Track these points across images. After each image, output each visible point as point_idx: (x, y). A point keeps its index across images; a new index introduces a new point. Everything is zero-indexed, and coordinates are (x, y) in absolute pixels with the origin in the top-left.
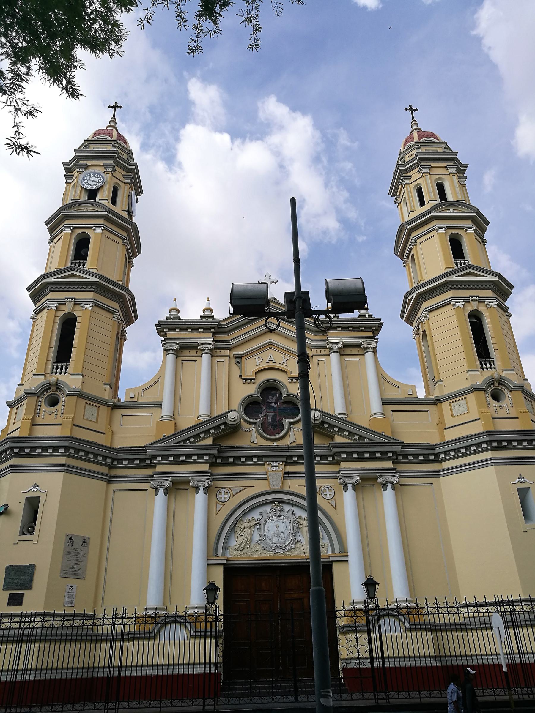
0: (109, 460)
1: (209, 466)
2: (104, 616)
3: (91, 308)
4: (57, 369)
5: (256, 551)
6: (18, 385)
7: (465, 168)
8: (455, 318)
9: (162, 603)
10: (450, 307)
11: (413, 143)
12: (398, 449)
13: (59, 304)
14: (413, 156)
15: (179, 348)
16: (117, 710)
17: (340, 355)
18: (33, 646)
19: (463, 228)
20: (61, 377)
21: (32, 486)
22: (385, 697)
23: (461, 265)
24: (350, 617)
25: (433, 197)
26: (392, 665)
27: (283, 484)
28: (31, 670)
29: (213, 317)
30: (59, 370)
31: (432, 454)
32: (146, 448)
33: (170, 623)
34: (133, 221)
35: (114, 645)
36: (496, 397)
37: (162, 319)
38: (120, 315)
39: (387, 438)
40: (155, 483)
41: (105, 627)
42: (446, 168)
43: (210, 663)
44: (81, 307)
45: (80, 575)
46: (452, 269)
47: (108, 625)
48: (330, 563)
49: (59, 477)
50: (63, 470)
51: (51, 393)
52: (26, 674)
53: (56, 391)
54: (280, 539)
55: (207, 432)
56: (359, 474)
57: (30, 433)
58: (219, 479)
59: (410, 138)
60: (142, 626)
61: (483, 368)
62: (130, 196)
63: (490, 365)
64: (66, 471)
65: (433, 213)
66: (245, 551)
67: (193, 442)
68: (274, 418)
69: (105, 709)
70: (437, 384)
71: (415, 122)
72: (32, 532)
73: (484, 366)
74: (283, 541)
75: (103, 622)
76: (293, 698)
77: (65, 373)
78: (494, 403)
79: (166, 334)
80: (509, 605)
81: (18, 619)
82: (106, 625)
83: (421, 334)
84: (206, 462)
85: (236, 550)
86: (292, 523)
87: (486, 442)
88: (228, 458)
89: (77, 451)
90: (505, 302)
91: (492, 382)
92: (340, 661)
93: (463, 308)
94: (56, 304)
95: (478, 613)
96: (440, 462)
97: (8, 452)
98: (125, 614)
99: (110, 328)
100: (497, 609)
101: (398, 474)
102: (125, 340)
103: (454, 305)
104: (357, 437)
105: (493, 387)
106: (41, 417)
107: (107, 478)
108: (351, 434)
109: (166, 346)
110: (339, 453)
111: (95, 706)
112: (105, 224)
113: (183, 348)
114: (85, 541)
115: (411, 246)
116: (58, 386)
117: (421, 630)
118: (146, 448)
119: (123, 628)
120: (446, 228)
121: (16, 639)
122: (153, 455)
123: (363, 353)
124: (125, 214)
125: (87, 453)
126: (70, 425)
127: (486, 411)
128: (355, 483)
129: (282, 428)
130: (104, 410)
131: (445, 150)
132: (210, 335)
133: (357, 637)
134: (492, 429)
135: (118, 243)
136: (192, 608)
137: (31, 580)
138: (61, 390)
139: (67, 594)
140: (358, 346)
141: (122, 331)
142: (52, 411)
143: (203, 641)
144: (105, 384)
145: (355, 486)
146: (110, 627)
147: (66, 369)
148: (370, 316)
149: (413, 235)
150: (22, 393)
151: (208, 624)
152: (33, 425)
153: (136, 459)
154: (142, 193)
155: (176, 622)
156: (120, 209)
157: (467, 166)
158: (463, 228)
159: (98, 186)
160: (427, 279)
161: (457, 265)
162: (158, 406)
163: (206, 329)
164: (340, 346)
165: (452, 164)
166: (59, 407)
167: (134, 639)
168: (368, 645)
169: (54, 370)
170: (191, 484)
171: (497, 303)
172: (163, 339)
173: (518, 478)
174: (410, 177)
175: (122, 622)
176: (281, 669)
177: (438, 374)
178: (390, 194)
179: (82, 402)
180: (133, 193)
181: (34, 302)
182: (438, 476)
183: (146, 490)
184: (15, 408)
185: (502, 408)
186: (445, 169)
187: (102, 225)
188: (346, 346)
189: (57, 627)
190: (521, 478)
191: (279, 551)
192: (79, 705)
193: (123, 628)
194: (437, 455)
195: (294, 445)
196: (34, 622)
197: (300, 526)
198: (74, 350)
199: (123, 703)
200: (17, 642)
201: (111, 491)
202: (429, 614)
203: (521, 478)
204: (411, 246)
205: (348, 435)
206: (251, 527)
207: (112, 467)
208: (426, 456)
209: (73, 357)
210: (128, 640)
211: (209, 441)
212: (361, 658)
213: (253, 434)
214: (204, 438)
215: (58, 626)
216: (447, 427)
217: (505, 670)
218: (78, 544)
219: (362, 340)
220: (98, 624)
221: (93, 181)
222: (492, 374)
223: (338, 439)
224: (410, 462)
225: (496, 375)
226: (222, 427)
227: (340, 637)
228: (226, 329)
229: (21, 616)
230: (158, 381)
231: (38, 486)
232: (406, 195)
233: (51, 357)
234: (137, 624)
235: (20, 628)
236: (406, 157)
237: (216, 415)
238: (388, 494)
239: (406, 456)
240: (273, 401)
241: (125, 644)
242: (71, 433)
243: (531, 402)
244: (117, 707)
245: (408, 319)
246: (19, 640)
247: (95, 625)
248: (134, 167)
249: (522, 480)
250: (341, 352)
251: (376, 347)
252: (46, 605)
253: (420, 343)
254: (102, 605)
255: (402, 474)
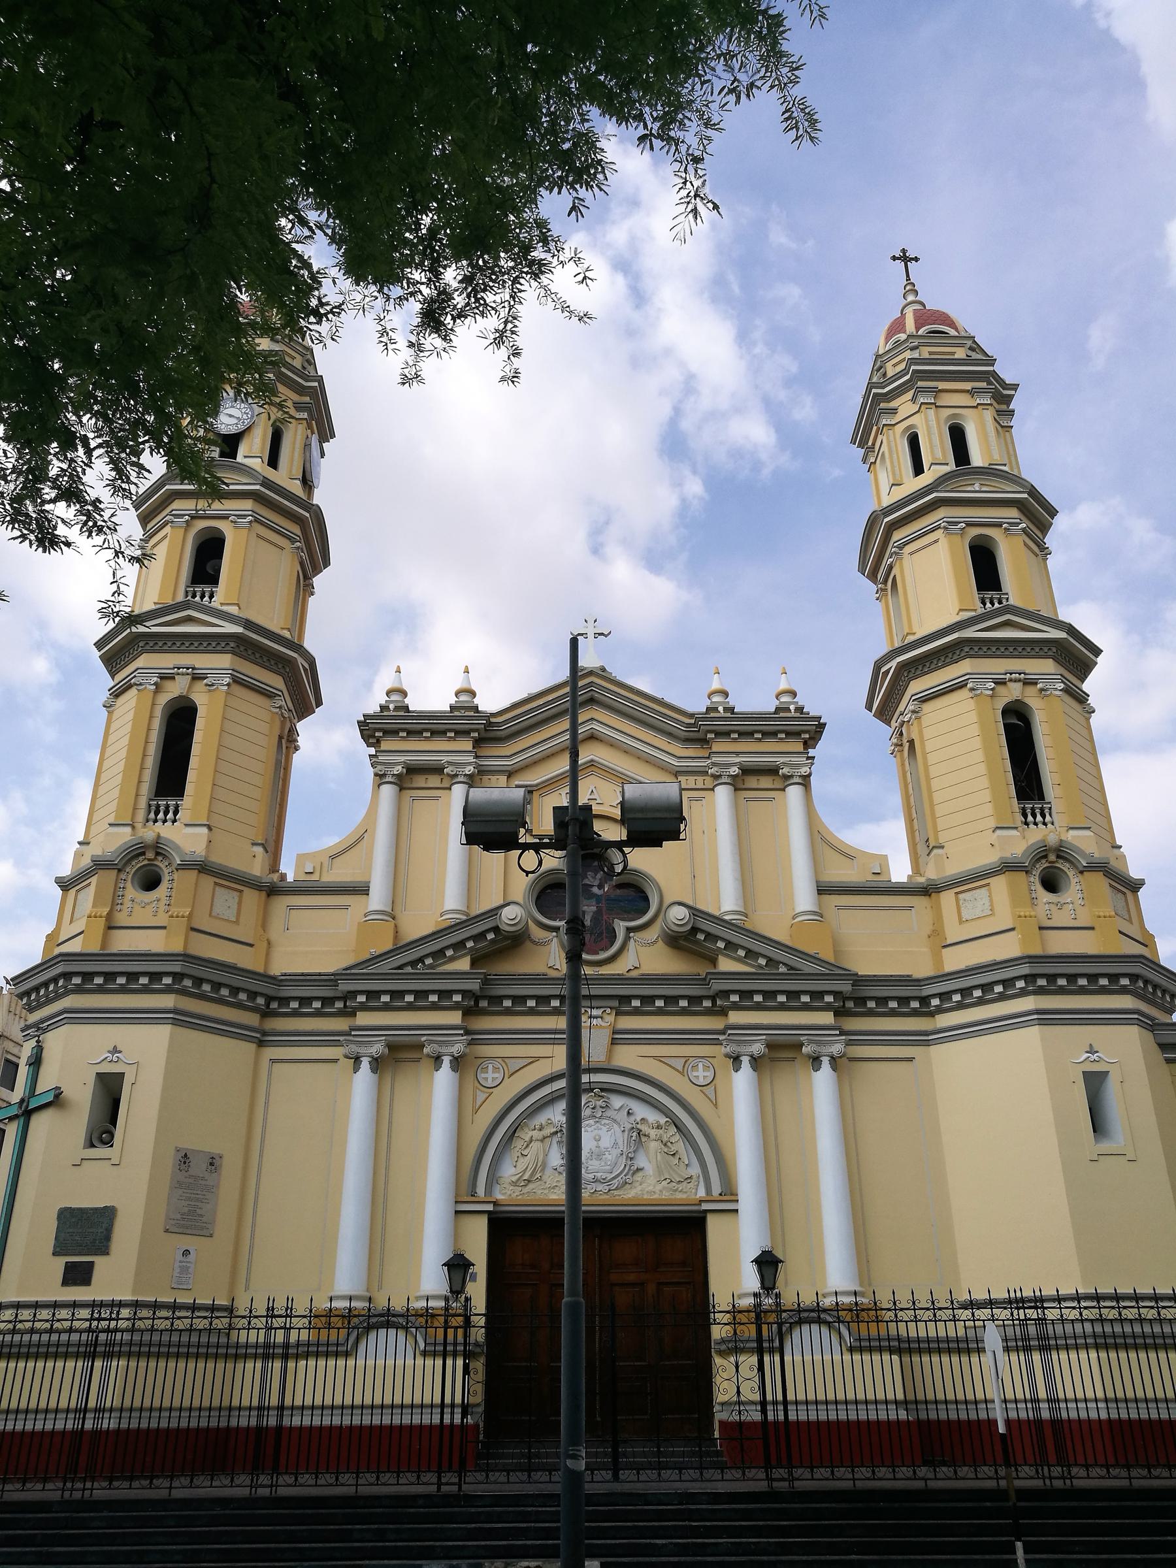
0: (261, 1001)
1: (464, 1015)
2: (251, 1311)
3: (226, 688)
4: (157, 813)
5: (554, 1188)
6: (80, 843)
7: (1013, 392)
8: (973, 717)
9: (365, 1288)
10: (964, 694)
11: (903, 337)
12: (846, 987)
13: (161, 678)
14: (902, 366)
15: (405, 770)
16: (274, 1488)
17: (736, 790)
18: (114, 1363)
19: (999, 525)
20: (165, 831)
21: (109, 1052)
22: (786, 1476)
23: (993, 604)
24: (726, 1324)
25: (939, 456)
26: (803, 1417)
27: (610, 1053)
28: (111, 1410)
29: (476, 709)
30: (161, 815)
31: (915, 998)
32: (337, 977)
33: (377, 1327)
34: (314, 503)
35: (270, 1365)
36: (1051, 884)
37: (371, 712)
38: (285, 701)
39: (823, 965)
40: (354, 1048)
41: (253, 1333)
42: (972, 393)
43: (453, 1406)
44: (207, 685)
45: (202, 1228)
46: (973, 614)
47: (258, 1329)
48: (701, 1215)
49: (162, 1033)
50: (170, 1021)
51: (146, 862)
52: (103, 1418)
53: (155, 859)
54: (603, 1164)
55: (459, 946)
56: (764, 1037)
57: (105, 942)
58: (484, 1042)
59: (897, 326)
60: (324, 1332)
61: (1027, 824)
62: (307, 446)
63: (1043, 816)
64: (175, 1022)
65: (937, 491)
66: (531, 1186)
67: (431, 966)
68: (596, 917)
69: (251, 1487)
70: (932, 854)
71: (911, 287)
72: (108, 1142)
73: (1030, 818)
74: (608, 1167)
75: (249, 1323)
76: (609, 1475)
77: (174, 821)
78: (1044, 896)
79: (378, 741)
80: (1036, 1308)
81: (85, 1313)
82: (254, 1328)
83: (906, 745)
84: (456, 1007)
85: (514, 1184)
86: (626, 1133)
87: (1024, 977)
88: (500, 999)
89: (198, 982)
90: (1083, 682)
91: (1042, 853)
92: (717, 1408)
93: (992, 696)
94: (155, 679)
95: (974, 1321)
96: (932, 1014)
97: (61, 983)
98: (291, 1309)
99: (264, 727)
100: (1012, 1314)
101: (844, 1037)
102: (297, 749)
103: (972, 689)
104: (762, 961)
105: (1044, 864)
106: (125, 912)
107: (258, 1035)
108: (751, 954)
109: (379, 767)
110: (726, 994)
111: (232, 1481)
112: (255, 510)
113: (413, 770)
114: (213, 1162)
115: (891, 560)
116: (158, 848)
117: (880, 1350)
118: (337, 977)
119: (287, 1336)
120: (964, 525)
121: (82, 1349)
122: (349, 992)
123: (782, 787)
124: (296, 488)
125: (217, 986)
126: (183, 929)
127: (1027, 914)
128: (756, 1053)
129: (613, 937)
130: (252, 898)
131: (970, 353)
132: (468, 745)
133: (737, 1363)
134: (1036, 950)
135: (282, 549)
136: (342, 1298)
137: (107, 1237)
138: (165, 857)
139: (177, 1264)
140: (772, 771)
141: (289, 731)
142: (146, 901)
143: (439, 1362)
144: (253, 844)
145: (756, 1062)
146: (262, 1332)
147: (176, 812)
148: (800, 709)
149: (897, 536)
150: (86, 862)
151: (960, 1324)
152: (110, 928)
153: (317, 998)
154: (333, 436)
155: (388, 1325)
156: (286, 476)
157: (1015, 387)
158: (999, 525)
159: (241, 427)
160: (921, 633)
161: (984, 603)
162: (362, 890)
163: (461, 733)
164: (735, 770)
165: (984, 385)
166: (161, 891)
167: (307, 1356)
168: (757, 1379)
169: (152, 815)
170: (425, 1050)
171: (1062, 686)
172: (372, 751)
173: (1087, 1052)
174: (894, 411)
175: (285, 1324)
176: (599, 1419)
177: (936, 832)
178: (853, 442)
179: (208, 881)
180: (315, 439)
181: (110, 672)
182: (927, 1043)
183: (336, 1061)
184: (72, 892)
185: (1060, 906)
186: (968, 396)
187: (250, 513)
188: (748, 771)
189: (162, 1331)
190: (1092, 1051)
191: (600, 1187)
192: (202, 1478)
193: (287, 1336)
194: (925, 1001)
195: (634, 974)
196: (117, 1319)
197: (644, 1139)
198: (191, 776)
199: (286, 1477)
200: (85, 1356)
201: (265, 1064)
202: (916, 1321)
203: (1092, 1051)
204: (891, 560)
205: (745, 957)
206: (545, 1138)
207: (266, 1014)
208: (904, 1001)
209: (189, 788)
210: (297, 1357)
211: (464, 964)
212: (743, 1403)
213: (552, 951)
214: (452, 959)
215: (162, 1327)
216: (949, 942)
217: (1002, 1429)
218: (198, 1167)
219: (781, 760)
220: (240, 1326)
221: (231, 416)
222: (1045, 836)
223: (726, 965)
224: (871, 1013)
225: (1052, 840)
226: (491, 936)
227: (718, 1361)
228: (502, 733)
229: (93, 1305)
230: (361, 838)
231: (120, 1052)
232: (884, 448)
233: (146, 788)
234: (314, 1328)
235: (89, 1330)
236: (889, 365)
237: (478, 912)
238: (823, 1080)
239: (862, 1001)
240: (596, 883)
241: (291, 1364)
242: (186, 945)
243: (1124, 894)
244: (274, 1483)
245: (881, 713)
246: (90, 1353)
247: (234, 1329)
248: (316, 384)
249: (1095, 1057)
250: (737, 784)
251: (810, 775)
252: (138, 1285)
253: (903, 765)
254: (247, 1288)
255: (853, 1038)
